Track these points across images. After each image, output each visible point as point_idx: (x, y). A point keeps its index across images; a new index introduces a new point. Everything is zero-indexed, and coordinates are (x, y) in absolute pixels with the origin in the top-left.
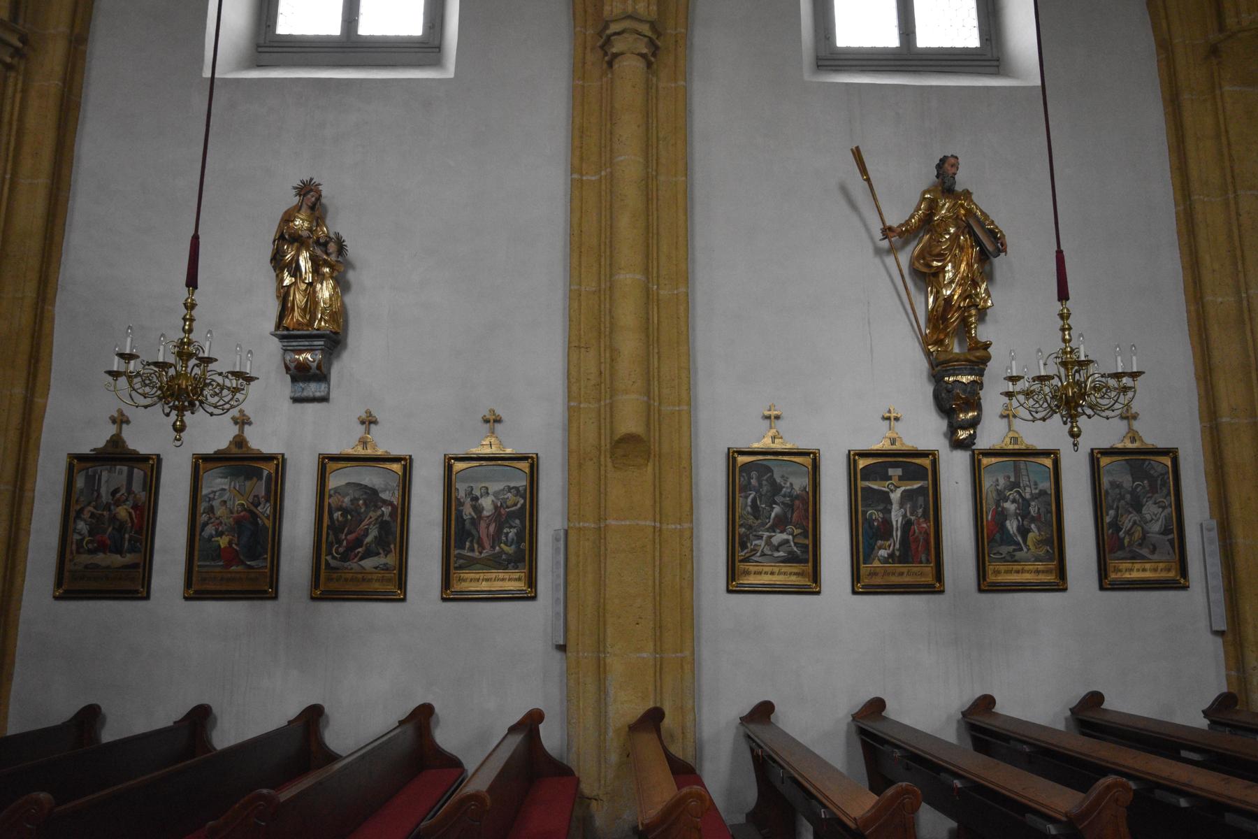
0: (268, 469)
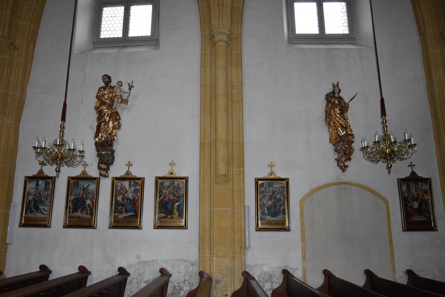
0: (140, 182)
